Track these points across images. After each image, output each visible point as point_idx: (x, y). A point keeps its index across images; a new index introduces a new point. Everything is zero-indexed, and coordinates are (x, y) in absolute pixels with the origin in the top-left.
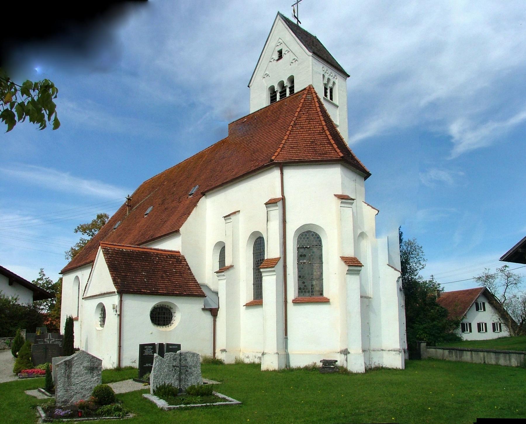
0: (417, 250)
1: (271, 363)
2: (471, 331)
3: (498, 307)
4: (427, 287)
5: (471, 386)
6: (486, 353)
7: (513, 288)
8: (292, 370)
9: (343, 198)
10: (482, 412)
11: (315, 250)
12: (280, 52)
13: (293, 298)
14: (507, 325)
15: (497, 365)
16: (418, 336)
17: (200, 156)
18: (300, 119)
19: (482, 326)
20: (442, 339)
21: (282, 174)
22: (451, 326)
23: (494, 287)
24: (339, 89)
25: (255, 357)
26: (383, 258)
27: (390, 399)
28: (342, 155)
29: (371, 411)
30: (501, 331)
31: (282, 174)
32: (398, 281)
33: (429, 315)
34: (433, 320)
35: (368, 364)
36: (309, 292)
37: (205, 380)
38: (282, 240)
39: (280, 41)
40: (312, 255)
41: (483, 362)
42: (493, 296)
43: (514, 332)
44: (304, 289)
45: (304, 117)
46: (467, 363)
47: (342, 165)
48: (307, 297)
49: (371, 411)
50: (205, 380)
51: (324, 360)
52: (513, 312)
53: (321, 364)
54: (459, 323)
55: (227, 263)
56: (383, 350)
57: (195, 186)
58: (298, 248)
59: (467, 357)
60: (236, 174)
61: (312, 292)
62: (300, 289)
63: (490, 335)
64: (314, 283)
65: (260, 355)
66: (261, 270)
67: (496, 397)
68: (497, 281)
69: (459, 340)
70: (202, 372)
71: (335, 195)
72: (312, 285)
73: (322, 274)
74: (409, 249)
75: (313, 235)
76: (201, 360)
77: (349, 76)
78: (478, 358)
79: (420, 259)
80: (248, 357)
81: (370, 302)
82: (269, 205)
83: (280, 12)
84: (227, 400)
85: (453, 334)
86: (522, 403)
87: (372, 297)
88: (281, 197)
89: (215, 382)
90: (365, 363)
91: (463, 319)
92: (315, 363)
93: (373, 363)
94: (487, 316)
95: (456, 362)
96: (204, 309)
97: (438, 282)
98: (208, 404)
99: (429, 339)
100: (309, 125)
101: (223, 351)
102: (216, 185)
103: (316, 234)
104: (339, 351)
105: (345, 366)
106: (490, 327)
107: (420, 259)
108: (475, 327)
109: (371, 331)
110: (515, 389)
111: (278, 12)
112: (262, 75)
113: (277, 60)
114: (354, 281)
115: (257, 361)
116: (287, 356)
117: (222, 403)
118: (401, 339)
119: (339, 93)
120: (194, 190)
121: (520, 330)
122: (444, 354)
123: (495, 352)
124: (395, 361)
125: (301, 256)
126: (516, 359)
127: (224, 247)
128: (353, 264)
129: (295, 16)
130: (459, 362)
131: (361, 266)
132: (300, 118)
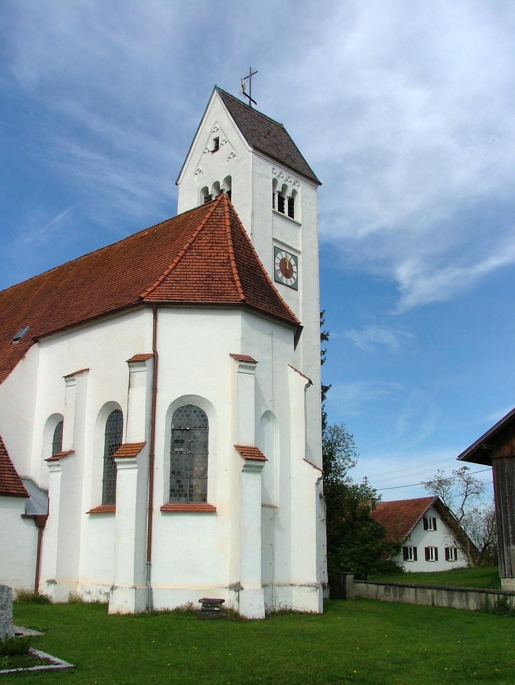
0: (346, 440)
1: (124, 603)
2: (416, 559)
3: (453, 525)
4: (358, 493)
5: (413, 638)
6: (435, 591)
7: (474, 499)
8: (156, 614)
9: (245, 361)
10: (427, 676)
11: (198, 434)
12: (217, 140)
13: (162, 505)
14: (464, 551)
15: (450, 608)
16: (342, 564)
17: (35, 283)
18: (199, 242)
19: (431, 553)
20: (376, 569)
21: (155, 318)
22: (389, 551)
23: (448, 496)
24: (302, 201)
25: (101, 593)
26: (297, 449)
27: (299, 659)
28: (242, 297)
29: (271, 678)
30: (456, 559)
31: (155, 318)
32: (317, 484)
33: (359, 534)
34: (365, 542)
35: (269, 605)
36: (186, 495)
37: (19, 630)
38: (149, 417)
39: (217, 126)
40: (192, 442)
41: (430, 604)
42: (447, 509)
43: (474, 561)
44: (179, 491)
45: (206, 239)
46: (409, 604)
47: (243, 310)
48: (182, 503)
49: (271, 678)
50: (19, 630)
51: (204, 599)
52: (474, 532)
53: (200, 606)
54: (400, 547)
55: (66, 447)
56: (292, 585)
57: (23, 328)
58: (173, 430)
59: (410, 595)
60: (88, 314)
61: (191, 496)
62: (172, 490)
63: (442, 565)
64: (194, 483)
65: (108, 590)
66: (116, 460)
67: (447, 654)
68: (453, 488)
69: (399, 571)
70: (16, 615)
71: (231, 355)
72: (191, 486)
73: (206, 469)
74: (335, 438)
75: (195, 412)
76: (15, 596)
77: (320, 184)
78: (426, 597)
79: (350, 453)
80: (89, 593)
81: (275, 514)
82: (133, 364)
83: (218, 86)
84: (52, 663)
85: (391, 563)
86: (481, 662)
87: (278, 506)
88: (152, 352)
89: (34, 633)
90: (266, 605)
91: (406, 541)
92: (192, 604)
93: (278, 603)
94: (439, 538)
95: (395, 604)
96: (25, 517)
97: (374, 487)
98: (21, 669)
99: (358, 570)
100: (210, 251)
101: (52, 582)
102: (57, 328)
103: (201, 411)
104: (227, 585)
105: (236, 609)
106: (442, 554)
107: (350, 453)
108: (421, 553)
109: (276, 556)
110: (473, 642)
111: (216, 86)
112: (194, 170)
113: (213, 152)
114: (253, 482)
115: (103, 599)
116: (149, 592)
117: (42, 667)
118: (318, 568)
119: (303, 207)
120: (21, 333)
121: (482, 558)
122: (377, 592)
123: (448, 590)
124: (310, 601)
125: (176, 441)
126: (475, 600)
127: (62, 422)
128: (253, 457)
129: (244, 93)
130: (398, 602)
131: (264, 461)
132: (199, 240)
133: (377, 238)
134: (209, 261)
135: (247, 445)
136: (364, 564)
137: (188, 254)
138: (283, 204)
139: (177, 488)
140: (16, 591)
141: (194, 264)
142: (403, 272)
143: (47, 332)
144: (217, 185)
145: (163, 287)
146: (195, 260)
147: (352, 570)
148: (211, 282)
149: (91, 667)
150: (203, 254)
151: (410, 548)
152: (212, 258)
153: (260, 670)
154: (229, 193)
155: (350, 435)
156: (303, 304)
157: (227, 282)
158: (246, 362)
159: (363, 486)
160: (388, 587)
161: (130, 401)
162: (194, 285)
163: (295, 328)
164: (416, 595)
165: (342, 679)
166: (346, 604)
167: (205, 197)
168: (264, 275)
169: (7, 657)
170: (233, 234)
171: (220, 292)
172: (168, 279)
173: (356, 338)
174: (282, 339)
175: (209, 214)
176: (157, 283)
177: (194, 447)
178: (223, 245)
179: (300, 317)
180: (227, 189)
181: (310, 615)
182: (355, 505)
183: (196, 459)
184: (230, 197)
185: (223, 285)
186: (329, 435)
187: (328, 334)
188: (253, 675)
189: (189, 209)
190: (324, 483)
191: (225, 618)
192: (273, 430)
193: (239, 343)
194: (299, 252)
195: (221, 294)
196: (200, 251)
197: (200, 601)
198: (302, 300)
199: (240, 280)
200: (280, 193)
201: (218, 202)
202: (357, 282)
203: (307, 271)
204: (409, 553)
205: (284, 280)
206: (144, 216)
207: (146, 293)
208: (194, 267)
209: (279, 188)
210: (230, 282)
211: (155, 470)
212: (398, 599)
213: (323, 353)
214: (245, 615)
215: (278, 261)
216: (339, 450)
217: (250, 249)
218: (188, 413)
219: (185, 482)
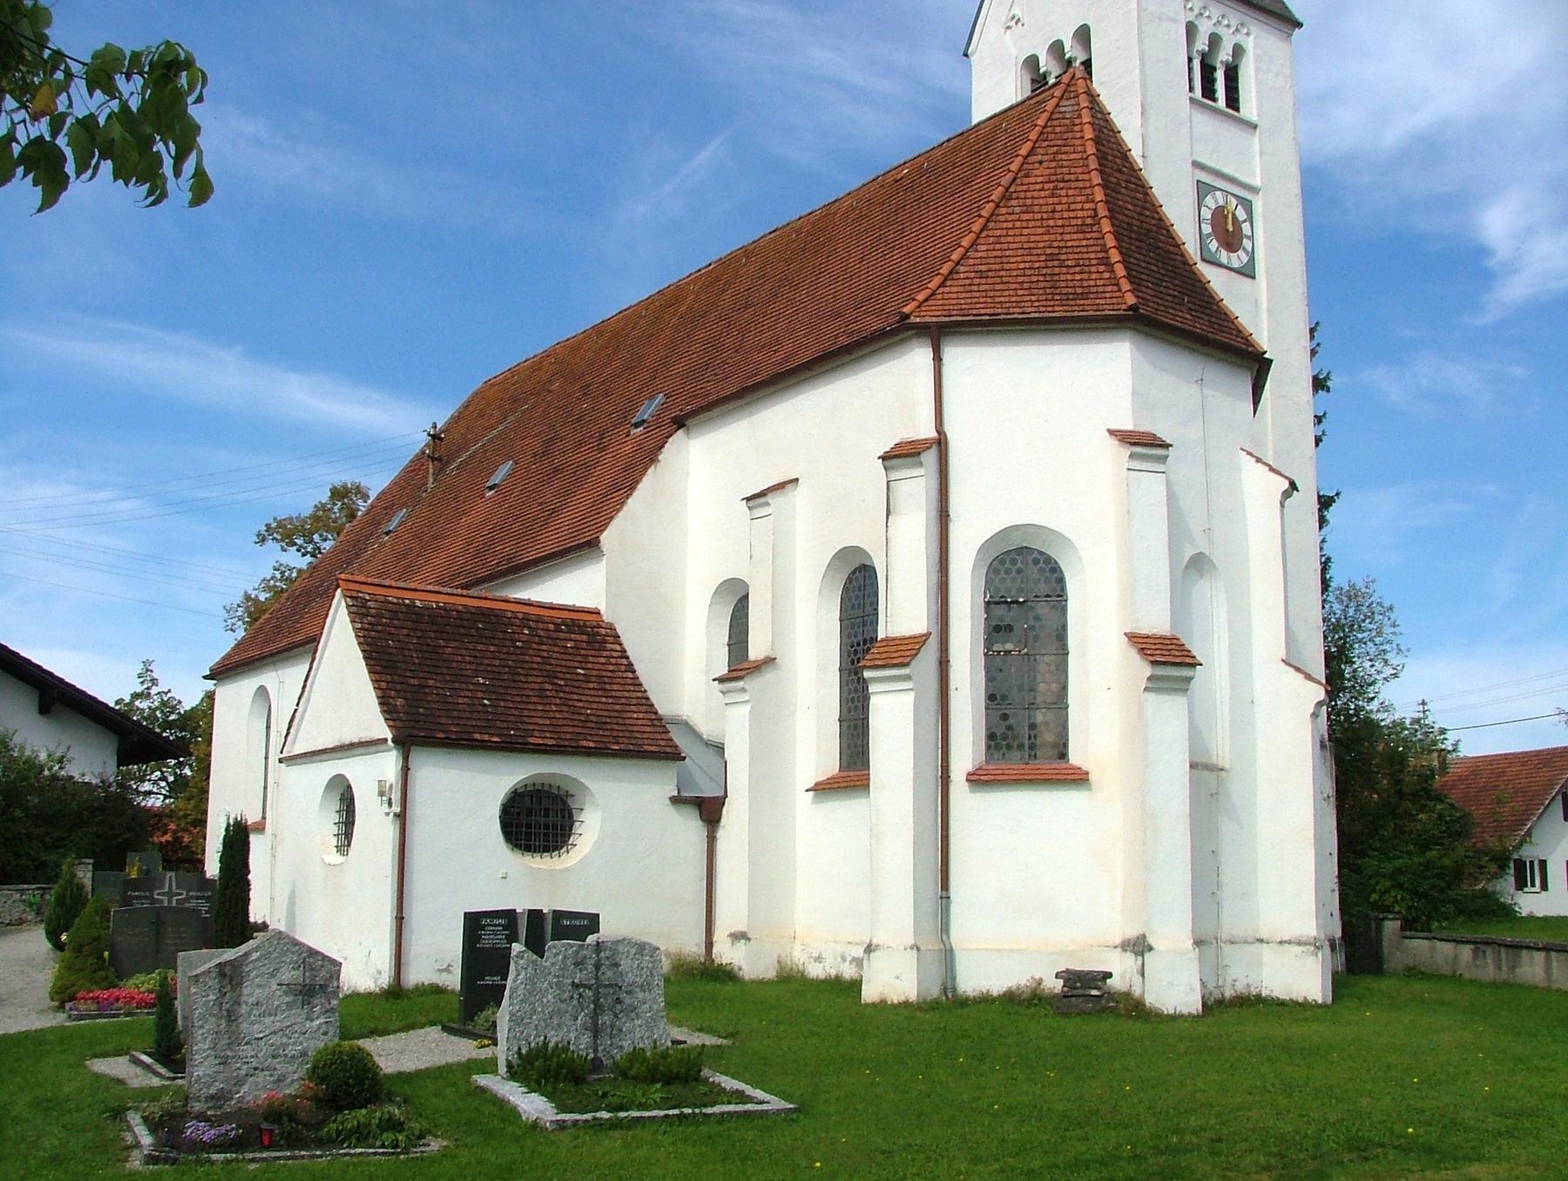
0: (1377, 617)
1: (893, 980)
2: (1544, 887)
8: (963, 1002)
9: (1143, 444)
13: (970, 768)
17: (669, 299)
18: (1026, 180)
21: (938, 359)
22: (1481, 867)
24: (1258, 70)
25: (844, 959)
26: (1267, 638)
27: (1283, 1102)
28: (1131, 300)
31: (938, 359)
32: (1315, 715)
34: (1424, 846)
35: (1211, 985)
36: (1021, 747)
37: (678, 1033)
38: (935, 578)
44: (1005, 737)
45: (1040, 173)
46: (1530, 988)
48: (1014, 763)
49: (1220, 1140)
50: (678, 1033)
51: (1067, 971)
53: (1057, 985)
54: (1508, 859)
55: (756, 652)
56: (1261, 941)
57: (652, 398)
58: (988, 604)
59: (1533, 968)
61: (1032, 747)
62: (991, 736)
64: (1039, 718)
65: (859, 952)
66: (867, 674)
69: (1507, 913)
70: (670, 1004)
71: (1112, 432)
72: (1033, 726)
74: (1351, 612)
75: (1036, 562)
76: (666, 965)
77: (1300, 25)
80: (819, 959)
81: (1220, 783)
84: (750, 1100)
85: (1485, 894)
87: (1227, 766)
90: (1203, 983)
91: (1521, 845)
92: (1040, 982)
93: (1229, 980)
98: (688, 1111)
99: (1409, 908)
100: (1051, 201)
101: (739, 936)
103: (1048, 560)
104: (1118, 941)
109: (1225, 877)
114: (1169, 712)
115: (848, 972)
117: (731, 1108)
119: (1259, 83)
120: (648, 411)
124: (1302, 976)
125: (997, 629)
128: (1168, 659)
130: (1506, 984)
131: (1193, 665)
132: (1027, 176)
133: (1429, 148)
134: (1051, 223)
135: (1155, 631)
136: (1425, 895)
137: (1003, 211)
138: (1213, 81)
139: (1003, 730)
140: (668, 955)
141: (1017, 232)
142: (1497, 223)
143: (704, 402)
144: (1057, 48)
145: (952, 288)
146: (1018, 224)
147: (1397, 909)
148: (1057, 271)
149: (831, 1109)
150: (1036, 209)
151: (1532, 863)
152: (1057, 215)
153: (1193, 1122)
154: (1087, 64)
155: (1387, 605)
156: (1268, 310)
157: (1093, 269)
158: (1146, 445)
159: (1417, 721)
160: (1482, 947)
161: (892, 543)
162: (1021, 279)
163: (1256, 366)
164: (1548, 968)
165: (1383, 1145)
166: (1385, 984)
167: (1033, 81)
168: (1178, 246)
169: (658, 1086)
170: (1101, 158)
171: (1079, 290)
172: (962, 269)
173: (1386, 382)
174: (1224, 391)
175: (1046, 115)
176: (937, 280)
177: (1036, 638)
178: (1080, 184)
179: (1263, 339)
180: (1081, 58)
181: (1304, 1006)
182: (1401, 763)
183: (1042, 667)
184: (1090, 73)
185: (1085, 276)
186: (1337, 607)
187: (1327, 378)
188: (1177, 1130)
189: (998, 110)
190: (1329, 714)
191: (1113, 1010)
192: (1211, 597)
193: (1127, 403)
194: (1254, 190)
195: (1084, 296)
196: (1029, 202)
197: (1057, 976)
198: (1267, 300)
199: (1124, 262)
200: (1204, 57)
201: (1062, 87)
202: (1395, 254)
203: (1276, 234)
204: (1528, 874)
205: (1224, 256)
206: (891, 136)
207: (914, 304)
208: (1018, 239)
209: (1202, 44)
210: (1102, 268)
211: (953, 694)
212: (1504, 976)
213: (1319, 420)
214: (1158, 1005)
215: (1207, 214)
216: (1360, 641)
217: (1143, 189)
218: (1019, 565)
219: (1019, 720)
